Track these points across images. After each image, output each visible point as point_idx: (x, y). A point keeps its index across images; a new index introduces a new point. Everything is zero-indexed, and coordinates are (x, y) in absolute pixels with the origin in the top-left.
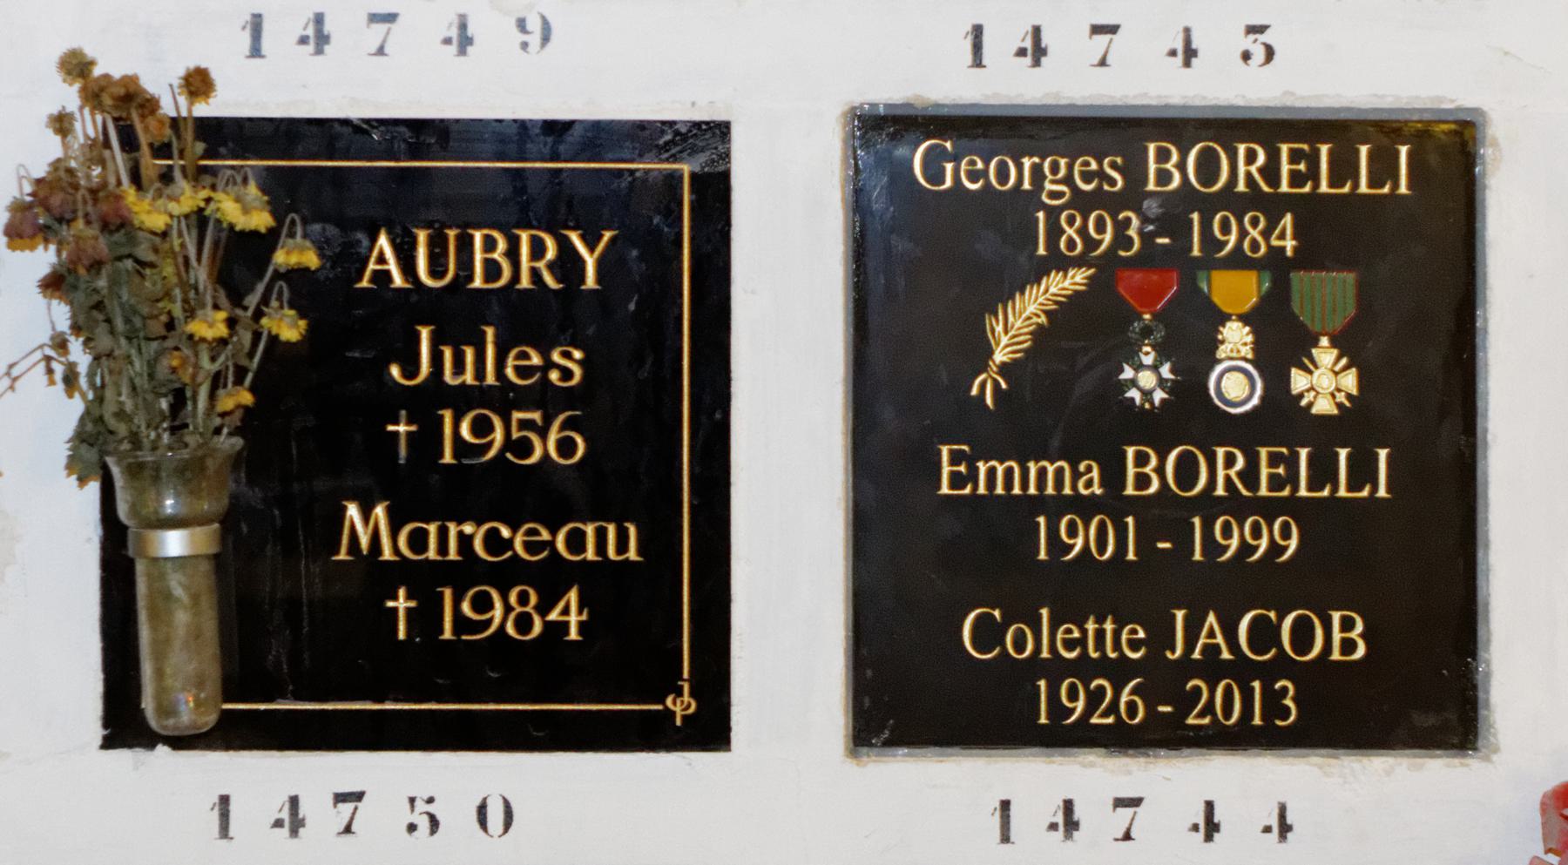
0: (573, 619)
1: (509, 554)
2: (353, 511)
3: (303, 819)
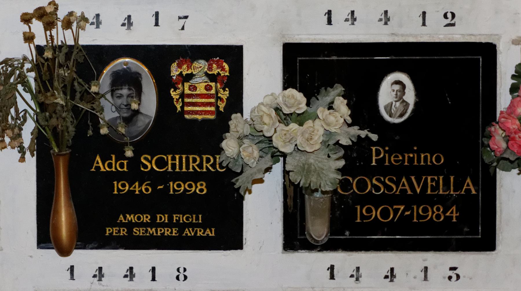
1: (352, 191)
3: (134, 275)
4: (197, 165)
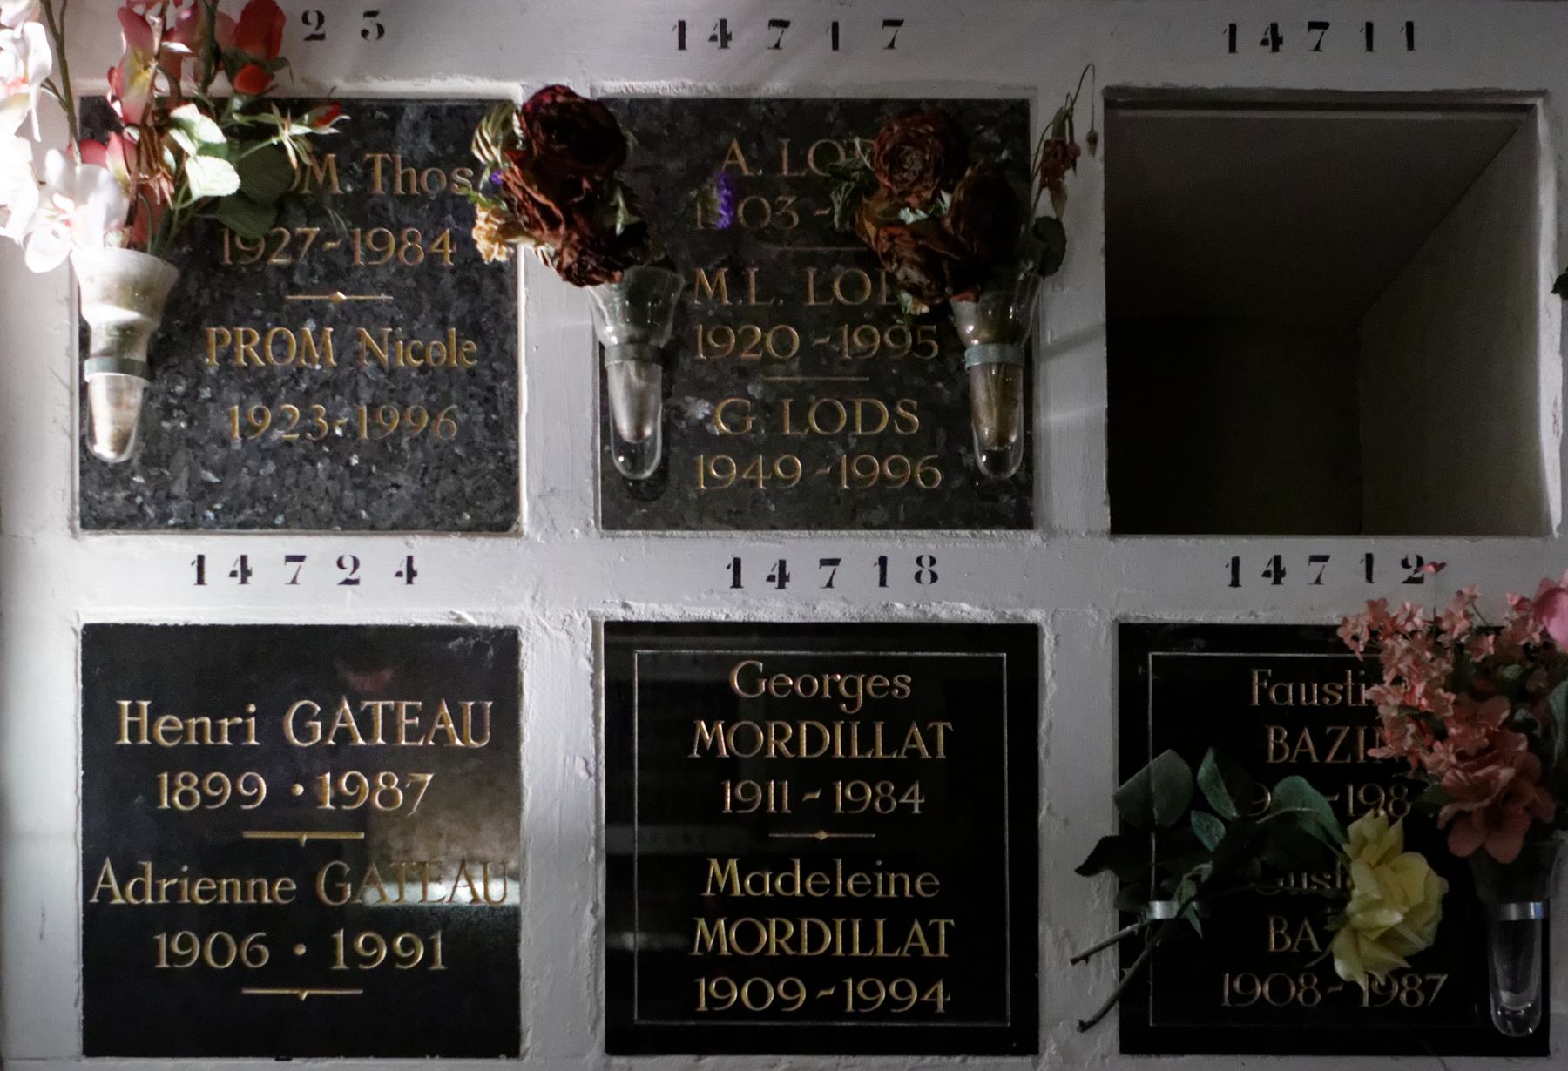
0: (917, 802)
2: (702, 923)
4: (788, 942)
